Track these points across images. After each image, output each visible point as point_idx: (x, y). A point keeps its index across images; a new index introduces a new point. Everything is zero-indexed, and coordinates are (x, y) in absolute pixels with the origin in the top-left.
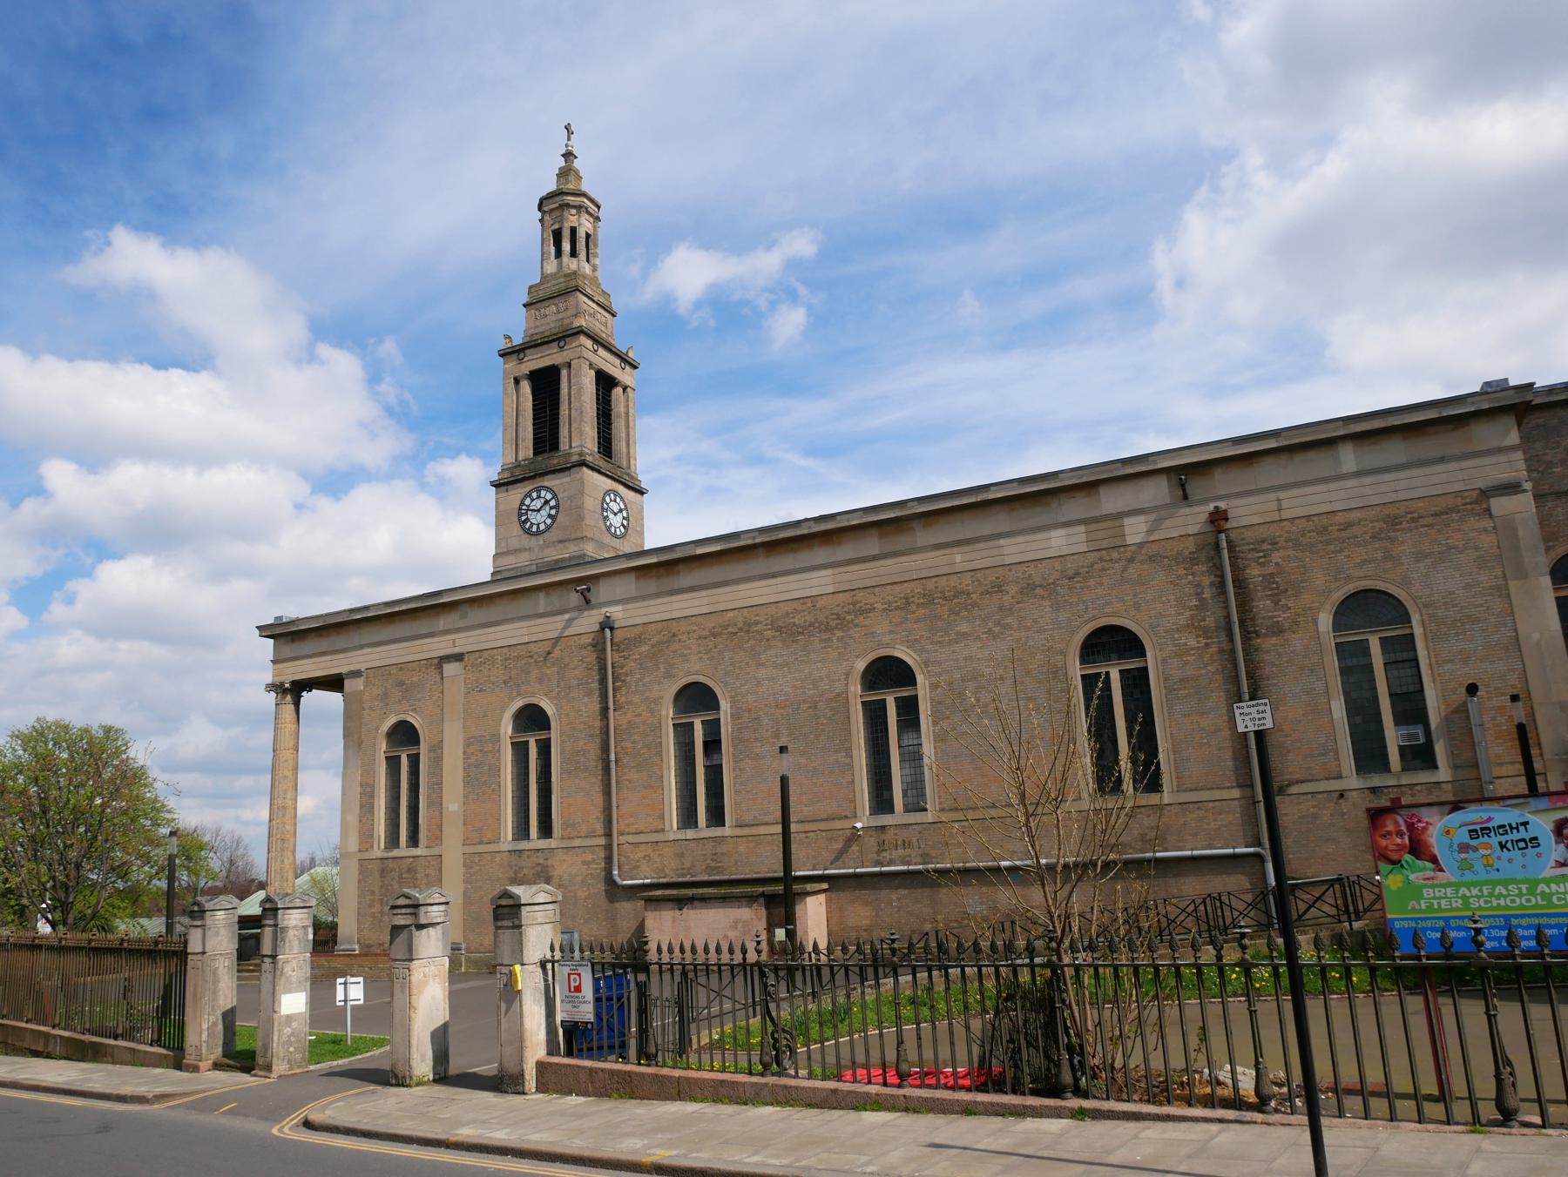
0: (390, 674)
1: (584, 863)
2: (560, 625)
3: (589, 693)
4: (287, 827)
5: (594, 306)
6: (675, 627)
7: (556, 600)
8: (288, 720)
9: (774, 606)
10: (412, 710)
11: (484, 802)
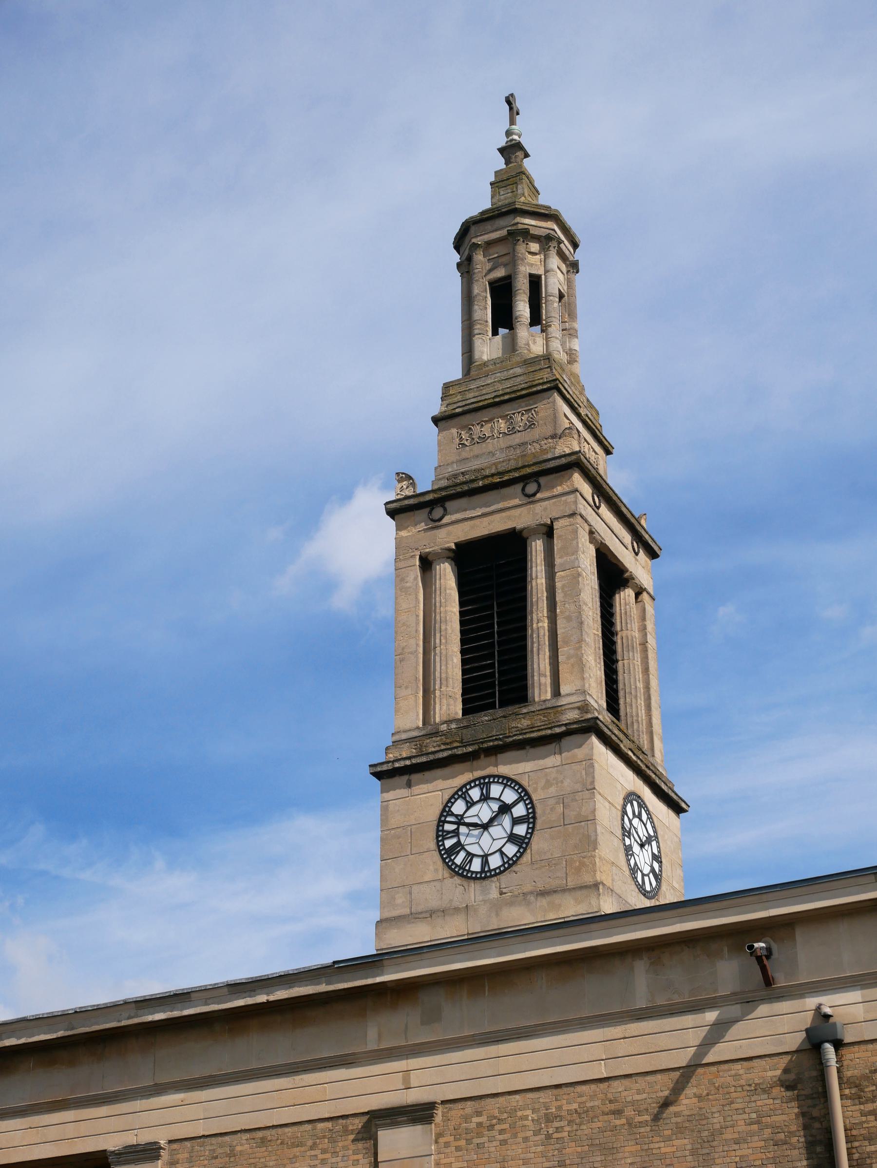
0: (232, 1154)
2: (695, 1038)
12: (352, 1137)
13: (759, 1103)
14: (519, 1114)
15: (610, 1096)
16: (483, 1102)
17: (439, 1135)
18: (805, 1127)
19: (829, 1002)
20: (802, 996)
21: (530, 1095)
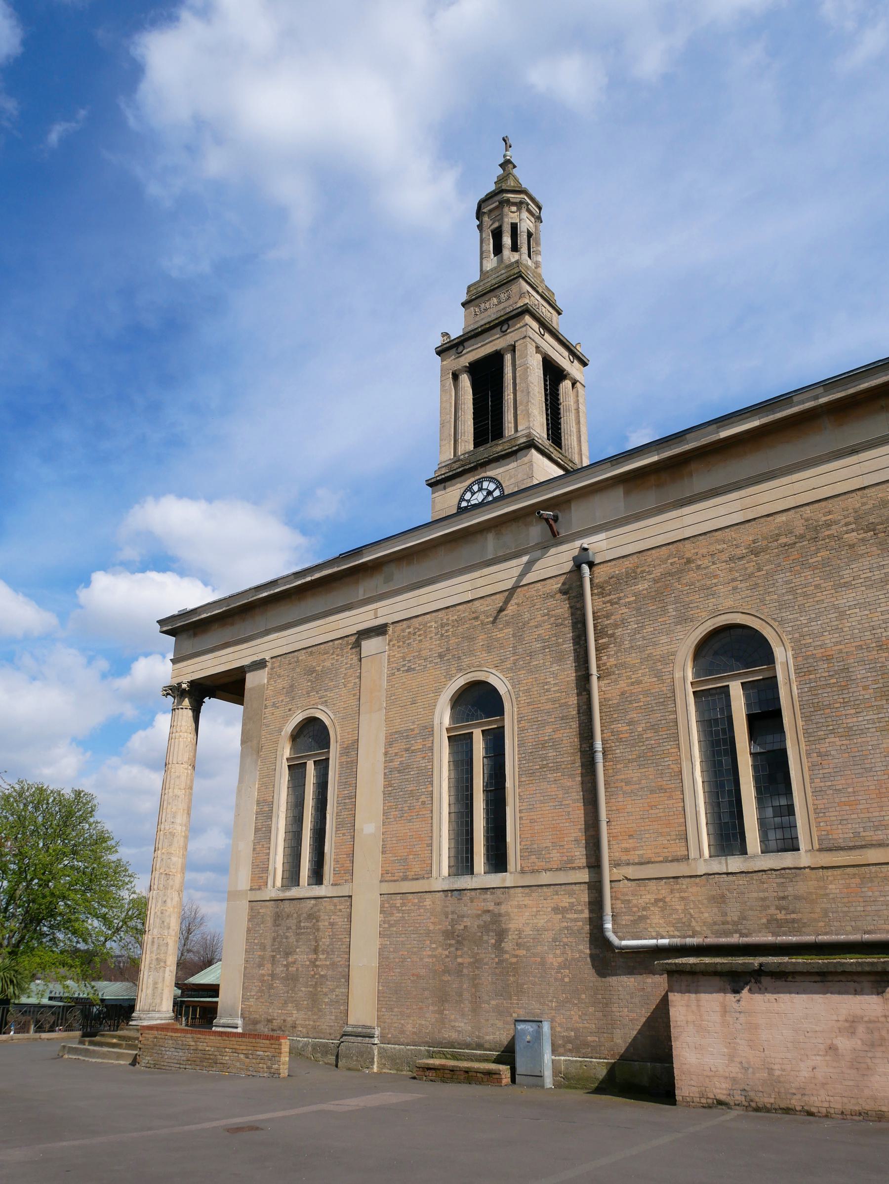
1: (556, 910)
2: (516, 572)
3: (559, 659)
4: (174, 859)
5: (539, 298)
6: (689, 550)
7: (510, 538)
8: (183, 729)
9: (857, 496)
10: (322, 704)
11: (410, 821)
12: (350, 646)
13: (549, 604)
14: (428, 625)
15: (473, 610)
16: (411, 621)
17: (390, 641)
18: (572, 614)
19: (585, 542)
20: (573, 540)
21: (434, 614)
